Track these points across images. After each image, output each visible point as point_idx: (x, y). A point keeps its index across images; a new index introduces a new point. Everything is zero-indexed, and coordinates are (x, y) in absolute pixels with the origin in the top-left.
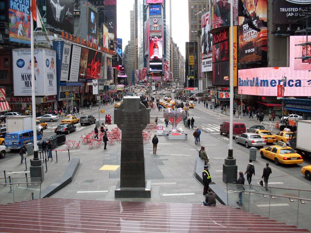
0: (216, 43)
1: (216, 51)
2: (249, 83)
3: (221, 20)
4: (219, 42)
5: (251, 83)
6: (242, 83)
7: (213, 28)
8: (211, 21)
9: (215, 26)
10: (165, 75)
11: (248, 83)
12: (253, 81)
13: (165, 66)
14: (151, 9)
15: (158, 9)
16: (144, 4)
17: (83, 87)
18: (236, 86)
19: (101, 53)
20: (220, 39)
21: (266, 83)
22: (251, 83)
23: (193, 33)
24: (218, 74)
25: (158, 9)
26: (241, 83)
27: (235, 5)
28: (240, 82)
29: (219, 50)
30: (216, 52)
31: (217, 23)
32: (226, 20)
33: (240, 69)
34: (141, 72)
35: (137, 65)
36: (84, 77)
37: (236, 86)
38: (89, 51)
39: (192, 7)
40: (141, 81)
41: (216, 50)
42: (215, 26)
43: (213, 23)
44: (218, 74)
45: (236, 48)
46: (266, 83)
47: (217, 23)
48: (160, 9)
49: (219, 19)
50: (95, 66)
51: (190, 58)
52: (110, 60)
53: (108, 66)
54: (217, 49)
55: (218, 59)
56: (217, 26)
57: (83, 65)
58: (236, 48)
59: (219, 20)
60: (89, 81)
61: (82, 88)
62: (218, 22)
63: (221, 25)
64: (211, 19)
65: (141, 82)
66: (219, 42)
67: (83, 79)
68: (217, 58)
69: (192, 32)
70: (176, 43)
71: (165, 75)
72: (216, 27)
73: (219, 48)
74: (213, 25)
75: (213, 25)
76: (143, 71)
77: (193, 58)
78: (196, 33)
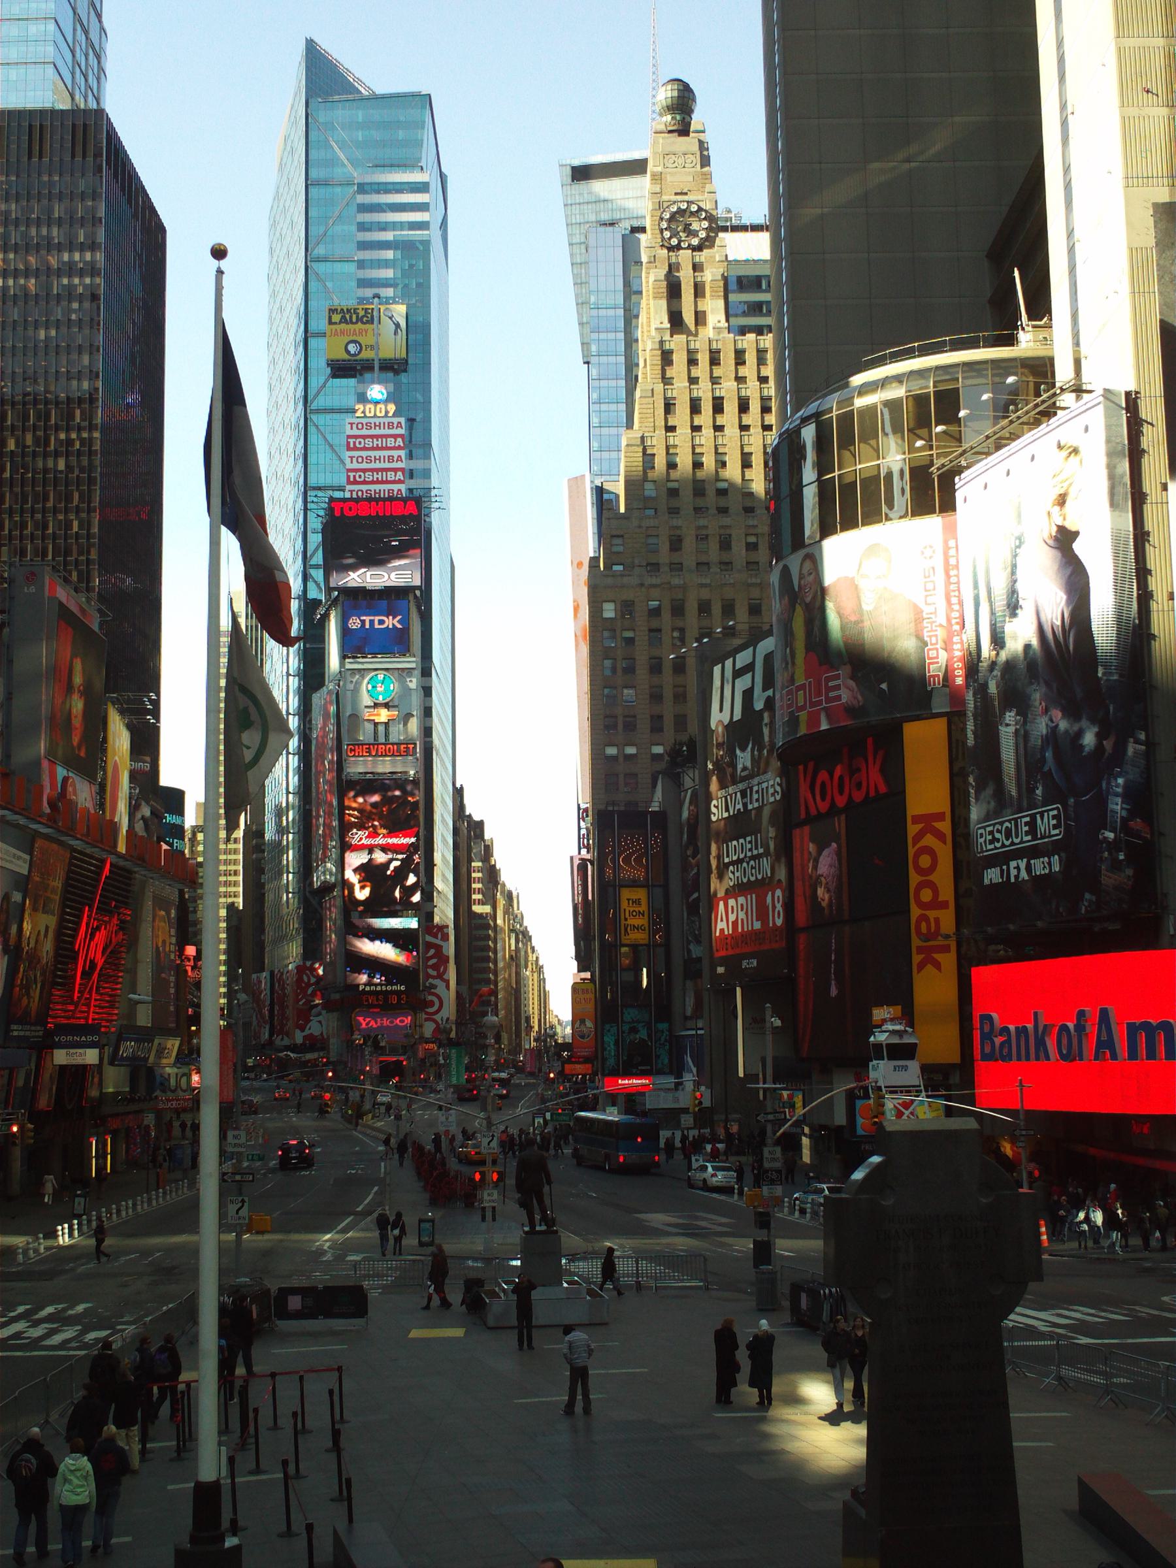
0: (814, 812)
1: (816, 861)
2: (1050, 1044)
3: (852, 683)
4: (833, 811)
5: (1065, 1041)
6: (1002, 1045)
7: (803, 730)
8: (789, 693)
9: (814, 720)
10: (432, 1004)
11: (1041, 1043)
12: (1080, 1028)
13: (432, 952)
14: (354, 623)
15: (390, 622)
16: (305, 591)
17: (28, 1075)
18: (955, 1058)
19: (129, 872)
20: (841, 793)
21: (1161, 1038)
22: (1065, 1041)
23: (614, 758)
24: (834, 992)
25: (390, 622)
26: (998, 1041)
27: (929, 600)
28: (987, 1037)
29: (838, 853)
30: (815, 867)
31: (828, 700)
32: (884, 686)
33: (984, 960)
34: (283, 989)
35: (260, 947)
36: (33, 1014)
37: (955, 1058)
38: (71, 864)
39: (609, 611)
40: (286, 1042)
41: (820, 853)
42: (814, 720)
43: (801, 703)
44: (834, 992)
45: (945, 843)
46: (1161, 1038)
47: (828, 700)
48: (406, 621)
49: (837, 677)
50: (93, 947)
51: (624, 904)
52: (168, 914)
53: (157, 948)
54: (826, 852)
55: (830, 904)
56: (828, 717)
57: (32, 945)
58: (945, 843)
59: (838, 687)
60: (63, 1039)
61: (21, 1083)
62: (831, 694)
63: (850, 710)
64: (792, 680)
65: (287, 1048)
66: (833, 811)
67: (32, 1024)
68: (824, 904)
69: (612, 751)
70: (476, 818)
71: (432, 1004)
72: (824, 726)
73: (834, 845)
74: (803, 715)
75: (803, 715)
76: (299, 980)
77: (644, 902)
78: (656, 758)
